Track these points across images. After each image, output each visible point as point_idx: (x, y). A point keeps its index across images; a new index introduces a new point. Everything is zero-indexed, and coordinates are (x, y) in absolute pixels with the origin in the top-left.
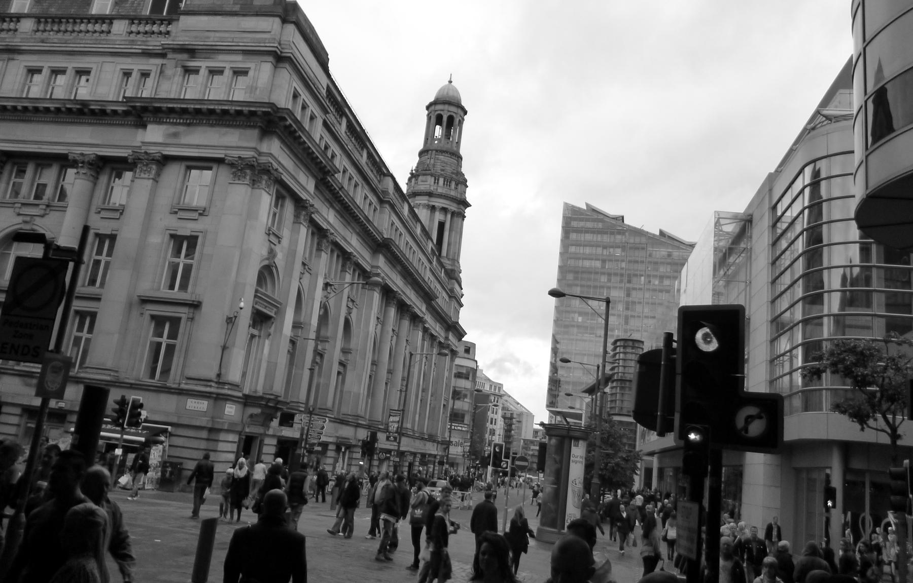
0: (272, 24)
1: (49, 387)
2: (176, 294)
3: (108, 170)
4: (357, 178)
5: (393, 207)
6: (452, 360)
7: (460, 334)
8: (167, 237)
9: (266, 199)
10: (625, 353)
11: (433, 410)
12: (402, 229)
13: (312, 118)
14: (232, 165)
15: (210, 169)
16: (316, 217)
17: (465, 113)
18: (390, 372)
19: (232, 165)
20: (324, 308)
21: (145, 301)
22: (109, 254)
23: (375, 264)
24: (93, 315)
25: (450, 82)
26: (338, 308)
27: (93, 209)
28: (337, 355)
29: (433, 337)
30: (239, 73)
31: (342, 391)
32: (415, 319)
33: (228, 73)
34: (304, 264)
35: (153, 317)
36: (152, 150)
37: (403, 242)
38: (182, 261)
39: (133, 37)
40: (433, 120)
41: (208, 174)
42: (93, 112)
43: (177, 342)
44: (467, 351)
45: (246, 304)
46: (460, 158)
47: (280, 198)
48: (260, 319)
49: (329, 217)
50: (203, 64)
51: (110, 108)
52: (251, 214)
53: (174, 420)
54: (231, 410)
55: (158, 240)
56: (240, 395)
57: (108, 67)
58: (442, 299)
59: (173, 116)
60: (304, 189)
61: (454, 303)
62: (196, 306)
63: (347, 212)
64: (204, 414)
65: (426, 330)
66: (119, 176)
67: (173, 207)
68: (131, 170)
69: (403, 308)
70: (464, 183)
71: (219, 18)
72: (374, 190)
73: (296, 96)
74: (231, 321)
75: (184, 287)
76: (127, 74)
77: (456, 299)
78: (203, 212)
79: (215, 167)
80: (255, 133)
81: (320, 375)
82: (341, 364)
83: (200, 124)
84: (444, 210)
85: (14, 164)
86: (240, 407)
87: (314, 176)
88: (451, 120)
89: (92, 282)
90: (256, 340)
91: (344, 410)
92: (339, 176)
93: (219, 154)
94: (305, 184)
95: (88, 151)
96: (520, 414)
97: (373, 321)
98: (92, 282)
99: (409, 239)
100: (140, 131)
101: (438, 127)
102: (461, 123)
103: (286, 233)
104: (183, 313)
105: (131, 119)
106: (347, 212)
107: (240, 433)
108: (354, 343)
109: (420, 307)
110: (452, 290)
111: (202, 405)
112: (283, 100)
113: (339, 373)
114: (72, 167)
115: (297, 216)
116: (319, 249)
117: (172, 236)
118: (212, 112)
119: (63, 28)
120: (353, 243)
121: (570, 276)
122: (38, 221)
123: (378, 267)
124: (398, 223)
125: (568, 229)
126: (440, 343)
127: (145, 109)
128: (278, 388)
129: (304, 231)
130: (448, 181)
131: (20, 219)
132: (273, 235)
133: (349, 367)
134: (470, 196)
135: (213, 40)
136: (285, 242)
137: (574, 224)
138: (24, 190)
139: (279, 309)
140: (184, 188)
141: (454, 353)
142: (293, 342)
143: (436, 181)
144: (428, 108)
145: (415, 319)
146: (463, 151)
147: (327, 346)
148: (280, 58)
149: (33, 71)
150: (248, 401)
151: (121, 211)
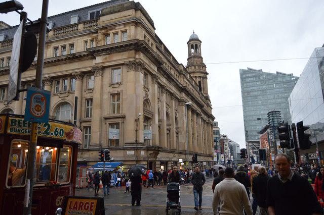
0: (131, 12)
1: (35, 113)
2: (116, 114)
3: (86, 76)
4: (170, 66)
5: (184, 75)
6: (212, 128)
7: (213, 118)
8: (109, 95)
9: (141, 75)
10: (273, 117)
11: (208, 146)
12: (188, 83)
13: (152, 45)
14: (127, 65)
15: (120, 68)
16: (159, 80)
17: (201, 42)
18: (193, 134)
19: (127, 65)
20: (167, 114)
21: (106, 119)
22: (91, 105)
23: (182, 96)
24: (90, 127)
25: (194, 33)
26: (172, 112)
27: (83, 91)
28: (175, 130)
29: (204, 121)
30: (124, 32)
31: (178, 143)
32: (198, 115)
33: (120, 33)
34: (158, 98)
35: (110, 124)
36: (99, 65)
37: (190, 87)
38: (116, 103)
39: (85, 29)
40: (190, 47)
41: (119, 70)
42: (77, 57)
43: (120, 102)
44: (215, 125)
45: (141, 113)
46: (202, 58)
47: (146, 74)
48: (147, 119)
49: (163, 81)
50: (111, 32)
51: (82, 54)
52: (136, 81)
53: (124, 159)
54: (143, 153)
55: (106, 97)
56: (145, 147)
57: (79, 41)
58: (205, 107)
59: (104, 52)
60: (154, 70)
61: (209, 108)
62: (124, 117)
63: (169, 78)
64: (133, 156)
65: (202, 118)
66: (90, 78)
67: (109, 84)
68: (93, 75)
69: (194, 112)
70: (205, 66)
71: (113, 15)
72: (177, 70)
73: (145, 37)
74: (137, 121)
75: (118, 112)
76: (86, 42)
77: (209, 106)
78: (120, 84)
79: (121, 67)
80: (133, 52)
81: (170, 138)
82: (177, 133)
83: (114, 53)
84: (200, 77)
85: (56, 81)
86: (146, 151)
87: (157, 66)
88: (196, 45)
89: (87, 116)
90: (146, 127)
91: (180, 149)
92: (164, 65)
93: (122, 62)
94: (154, 69)
95: (78, 71)
96: (235, 145)
97: (184, 117)
98: (87, 116)
99: (191, 86)
100: (94, 60)
101: (192, 49)
102: (200, 46)
103: (150, 87)
104: (119, 120)
105: (90, 57)
106: (169, 78)
107: (147, 161)
108: (180, 125)
109: (199, 111)
110: (208, 103)
111: (132, 152)
112: (141, 38)
113: (167, 134)
114: (74, 78)
115: (153, 81)
116: (162, 93)
117: (111, 94)
118: (117, 47)
119: (62, 31)
120: (173, 89)
121: (246, 94)
122: (66, 98)
123: (183, 97)
124: (187, 81)
125: (242, 79)
126: (207, 122)
127: (94, 52)
128: (157, 143)
129: (156, 86)
130: (199, 67)
131: (60, 99)
132: (146, 88)
133: (179, 134)
134: (208, 71)
135: (112, 22)
136: (150, 90)
137: (244, 76)
138: (60, 89)
139: (153, 115)
140: (112, 77)
141: (212, 125)
142: (159, 127)
143: (195, 67)
144: (187, 43)
145: (198, 115)
146: (202, 56)
147: (171, 127)
148: (137, 23)
149: (56, 48)
150: (148, 149)
151: (92, 89)
